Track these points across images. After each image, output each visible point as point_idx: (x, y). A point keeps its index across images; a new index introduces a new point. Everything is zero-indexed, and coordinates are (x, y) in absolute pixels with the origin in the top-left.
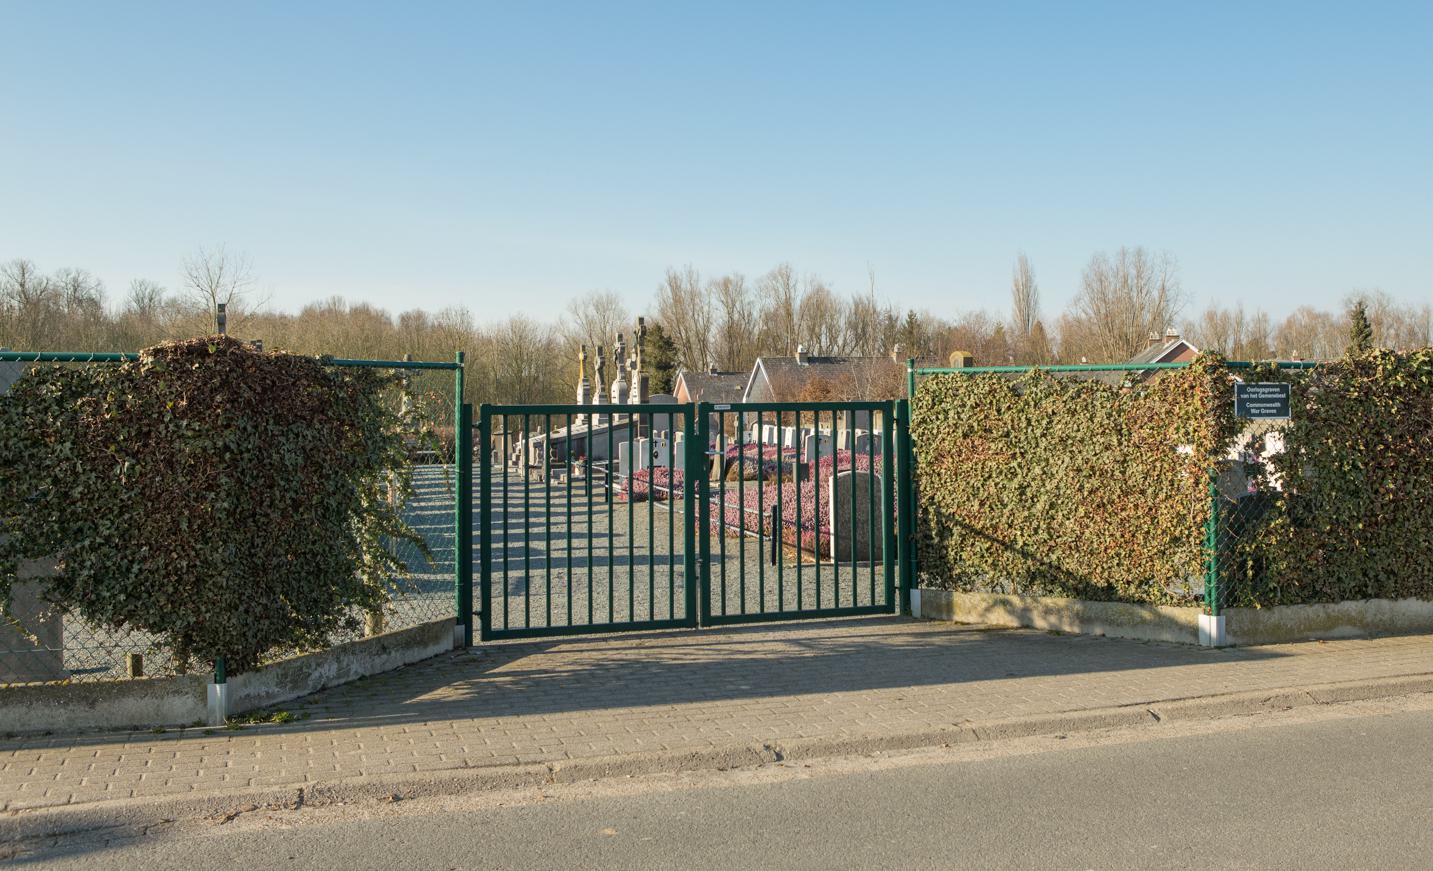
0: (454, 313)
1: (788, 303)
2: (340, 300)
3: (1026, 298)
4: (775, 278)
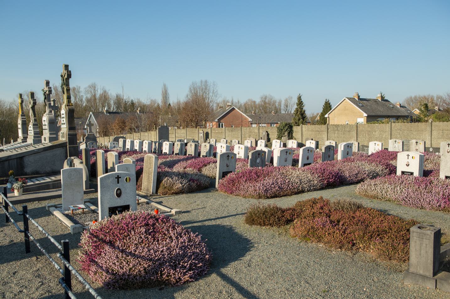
1: (95, 96)
3: (165, 95)
4: (90, 87)
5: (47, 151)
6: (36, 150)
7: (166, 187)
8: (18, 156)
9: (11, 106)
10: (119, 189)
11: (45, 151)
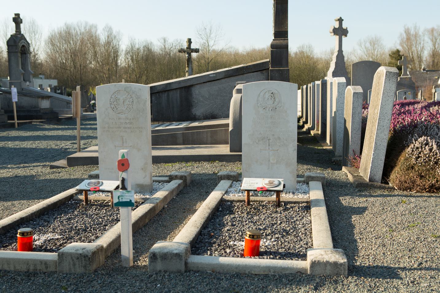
0: (305, 47)
2: (96, 27)
6: (212, 76)
7: (412, 168)
8: (183, 85)
9: (350, 57)
11: (228, 77)
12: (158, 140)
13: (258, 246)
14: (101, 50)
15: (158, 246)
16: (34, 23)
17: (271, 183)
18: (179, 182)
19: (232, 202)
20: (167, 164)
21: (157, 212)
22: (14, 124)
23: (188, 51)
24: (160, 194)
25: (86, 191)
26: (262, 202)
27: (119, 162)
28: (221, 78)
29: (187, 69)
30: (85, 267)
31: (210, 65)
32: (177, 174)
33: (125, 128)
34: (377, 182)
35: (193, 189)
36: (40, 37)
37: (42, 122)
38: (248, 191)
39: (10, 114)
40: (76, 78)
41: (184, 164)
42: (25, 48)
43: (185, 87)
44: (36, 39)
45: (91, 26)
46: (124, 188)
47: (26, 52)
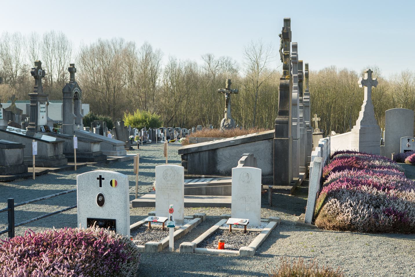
5: (247, 144)
6: (232, 142)
8: (210, 148)
10: (100, 195)
11: (244, 143)
12: (189, 191)
13: (223, 245)
14: (138, 71)
15: (184, 244)
16: (63, 38)
17: (242, 221)
18: (198, 219)
19: (223, 230)
20: (194, 208)
21: (185, 234)
22: (74, 166)
23: (228, 92)
24: (187, 226)
25: (150, 222)
26: (238, 231)
27: (170, 209)
28: (238, 143)
29: (226, 109)
30: (155, 250)
31: (260, 88)
32: (198, 214)
33: (170, 189)
34: (309, 223)
35: (206, 222)
36: (69, 54)
37: (94, 165)
38: (231, 225)
39: (70, 157)
40: (109, 101)
41: (204, 208)
42: (77, 94)
43: (212, 150)
44: (66, 57)
45: (130, 44)
46: (171, 220)
47: (78, 98)
